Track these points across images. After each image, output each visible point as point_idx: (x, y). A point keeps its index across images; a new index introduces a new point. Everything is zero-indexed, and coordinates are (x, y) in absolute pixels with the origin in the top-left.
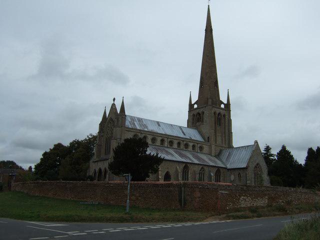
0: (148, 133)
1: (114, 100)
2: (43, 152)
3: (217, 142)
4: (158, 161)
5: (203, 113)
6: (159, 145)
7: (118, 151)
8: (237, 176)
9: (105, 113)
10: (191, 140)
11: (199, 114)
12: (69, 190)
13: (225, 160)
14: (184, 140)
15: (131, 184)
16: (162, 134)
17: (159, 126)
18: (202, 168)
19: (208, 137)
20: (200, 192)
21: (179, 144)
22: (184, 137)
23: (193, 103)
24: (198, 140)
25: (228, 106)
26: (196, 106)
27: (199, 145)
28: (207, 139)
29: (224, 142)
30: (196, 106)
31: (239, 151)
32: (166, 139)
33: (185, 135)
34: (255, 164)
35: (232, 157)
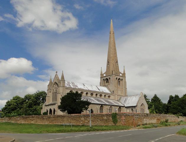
1: (57, 72)
2: (6, 101)
4: (88, 103)
5: (110, 78)
6: (85, 95)
7: (63, 99)
11: (107, 79)
12: (45, 119)
13: (123, 102)
14: (99, 93)
15: (91, 114)
16: (86, 90)
17: (84, 85)
18: (111, 107)
20: (124, 117)
22: (99, 91)
24: (96, 91)
25: (124, 74)
28: (112, 92)
29: (122, 93)
30: (105, 75)
31: (132, 97)
33: (99, 90)
35: (128, 100)
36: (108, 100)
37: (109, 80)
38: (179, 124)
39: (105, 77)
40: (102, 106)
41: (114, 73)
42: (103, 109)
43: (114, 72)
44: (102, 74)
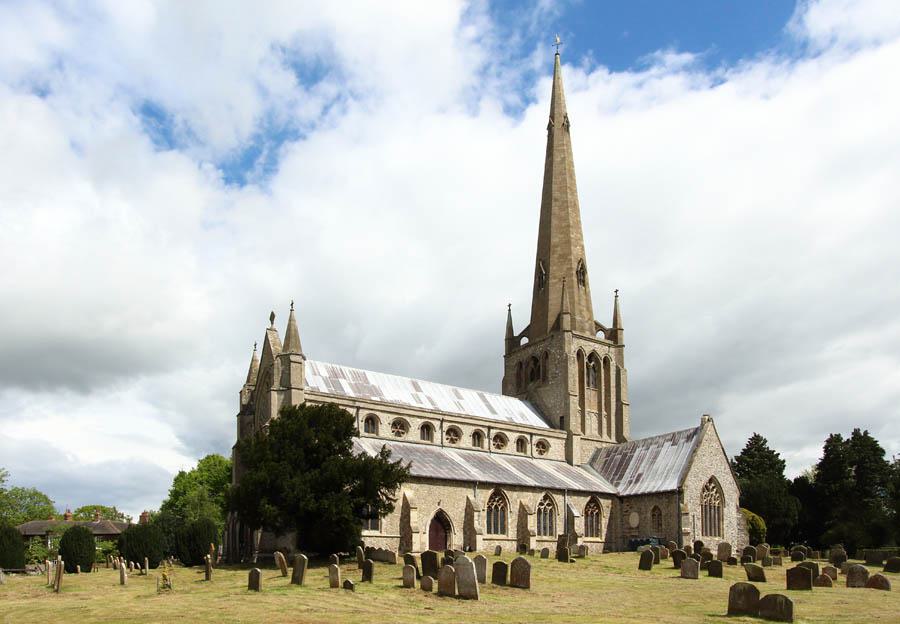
0: (379, 407)
3: (588, 431)
5: (546, 355)
6: (470, 446)
8: (649, 515)
10: (513, 426)
11: (535, 359)
18: (545, 498)
19: (562, 418)
21: (477, 436)
23: (516, 333)
24: (477, 414)
27: (536, 439)
28: (558, 421)
29: (605, 430)
30: (525, 341)
32: (436, 424)
34: (705, 480)
36: (534, 462)
37: (541, 362)
38: (43, 92)
39: (527, 346)
40: (499, 491)
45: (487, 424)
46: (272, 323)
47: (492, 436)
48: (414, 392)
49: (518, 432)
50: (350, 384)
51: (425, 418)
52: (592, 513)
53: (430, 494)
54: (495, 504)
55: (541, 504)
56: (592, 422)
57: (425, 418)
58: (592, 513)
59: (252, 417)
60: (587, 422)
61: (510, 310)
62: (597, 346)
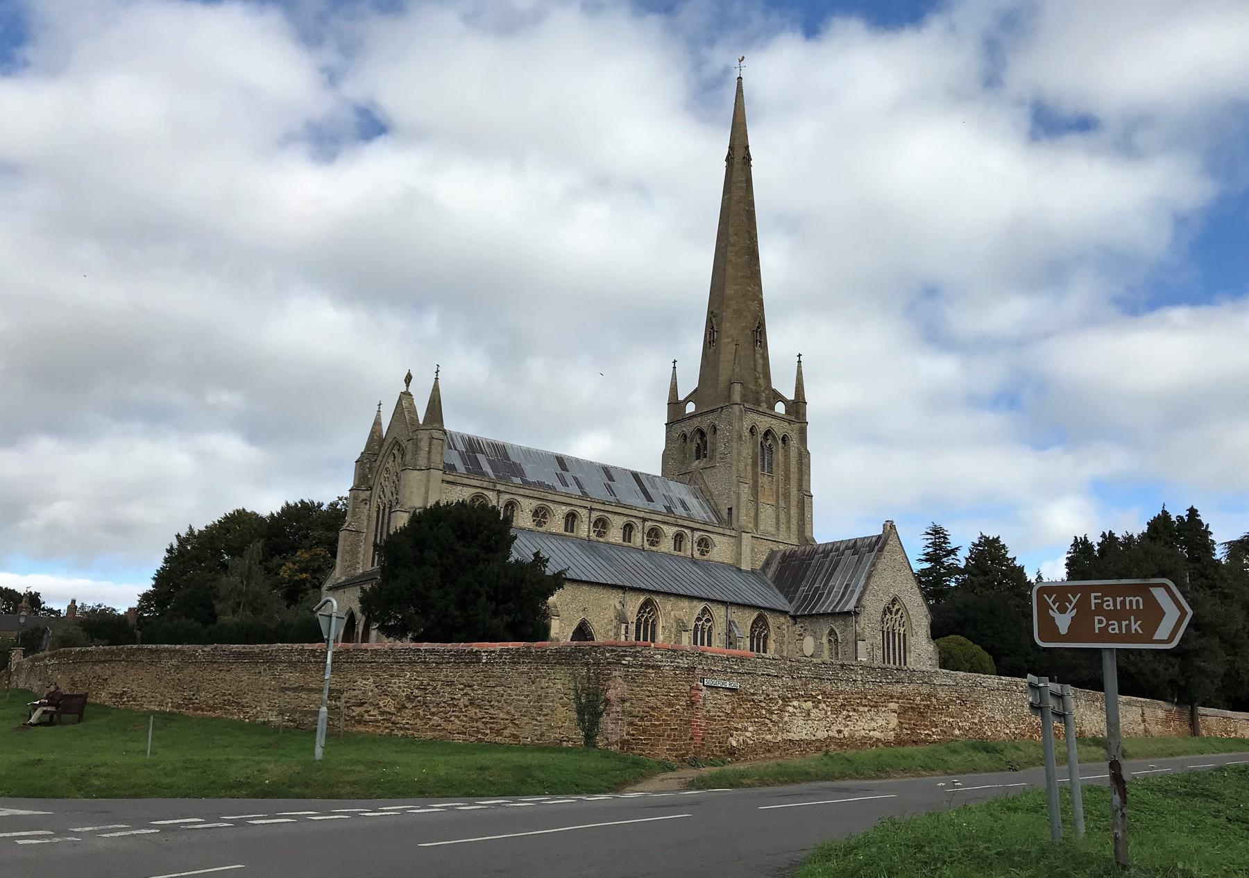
5: (715, 429)
6: (561, 530)
9: (377, 423)
11: (702, 433)
18: (705, 610)
23: (681, 398)
25: (797, 407)
26: (690, 408)
28: (725, 514)
30: (690, 408)
34: (887, 599)
37: (708, 437)
39: (692, 416)
41: (737, 397)
42: (654, 626)
43: (737, 388)
44: (675, 405)
45: (642, 514)
46: (408, 386)
47: (593, 520)
48: (560, 471)
49: (677, 525)
50: (489, 460)
51: (571, 505)
52: (760, 633)
53: (573, 599)
54: (646, 615)
55: (698, 619)
56: (767, 514)
57: (571, 505)
58: (760, 633)
59: (368, 493)
60: (762, 516)
61: (674, 367)
62: (774, 422)
